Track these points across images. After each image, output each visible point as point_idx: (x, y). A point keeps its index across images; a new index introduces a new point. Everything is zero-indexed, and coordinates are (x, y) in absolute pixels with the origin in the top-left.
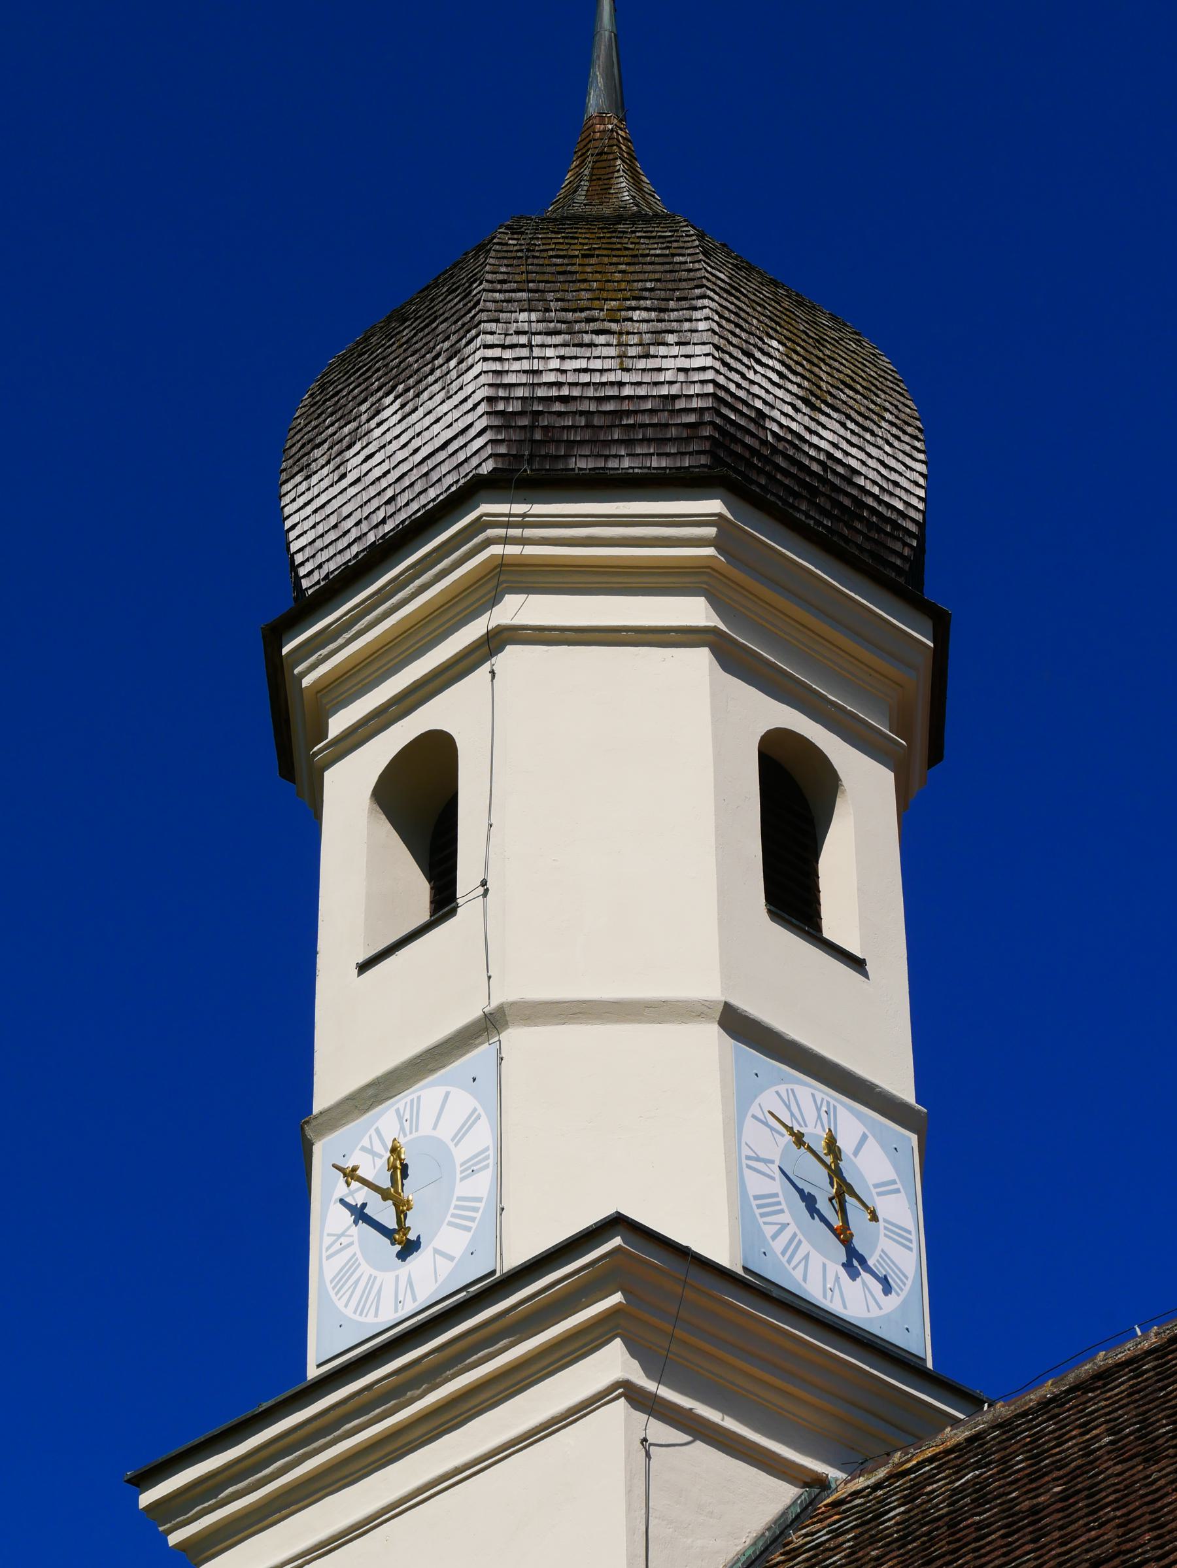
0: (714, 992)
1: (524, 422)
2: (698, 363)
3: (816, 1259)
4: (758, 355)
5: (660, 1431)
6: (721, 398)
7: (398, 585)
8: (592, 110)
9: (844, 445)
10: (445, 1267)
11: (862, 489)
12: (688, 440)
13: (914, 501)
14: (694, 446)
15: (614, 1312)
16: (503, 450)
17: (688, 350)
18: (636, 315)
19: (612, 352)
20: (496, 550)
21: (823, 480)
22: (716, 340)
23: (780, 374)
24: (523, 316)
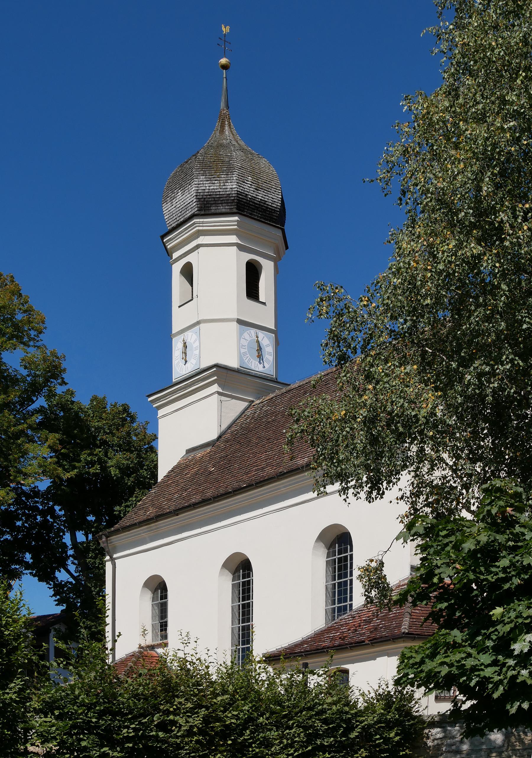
0: (235, 316)
1: (202, 200)
2: (234, 187)
3: (254, 361)
4: (246, 182)
5: (223, 398)
6: (239, 193)
7: (182, 232)
8: (222, 108)
9: (264, 196)
10: (192, 366)
11: (268, 205)
12: (232, 203)
13: (279, 204)
14: (233, 204)
15: (216, 379)
16: (199, 206)
17: (232, 184)
18: (222, 176)
19: (218, 185)
20: (197, 228)
21: (260, 205)
22: (237, 181)
23: (251, 185)
24: (202, 177)
